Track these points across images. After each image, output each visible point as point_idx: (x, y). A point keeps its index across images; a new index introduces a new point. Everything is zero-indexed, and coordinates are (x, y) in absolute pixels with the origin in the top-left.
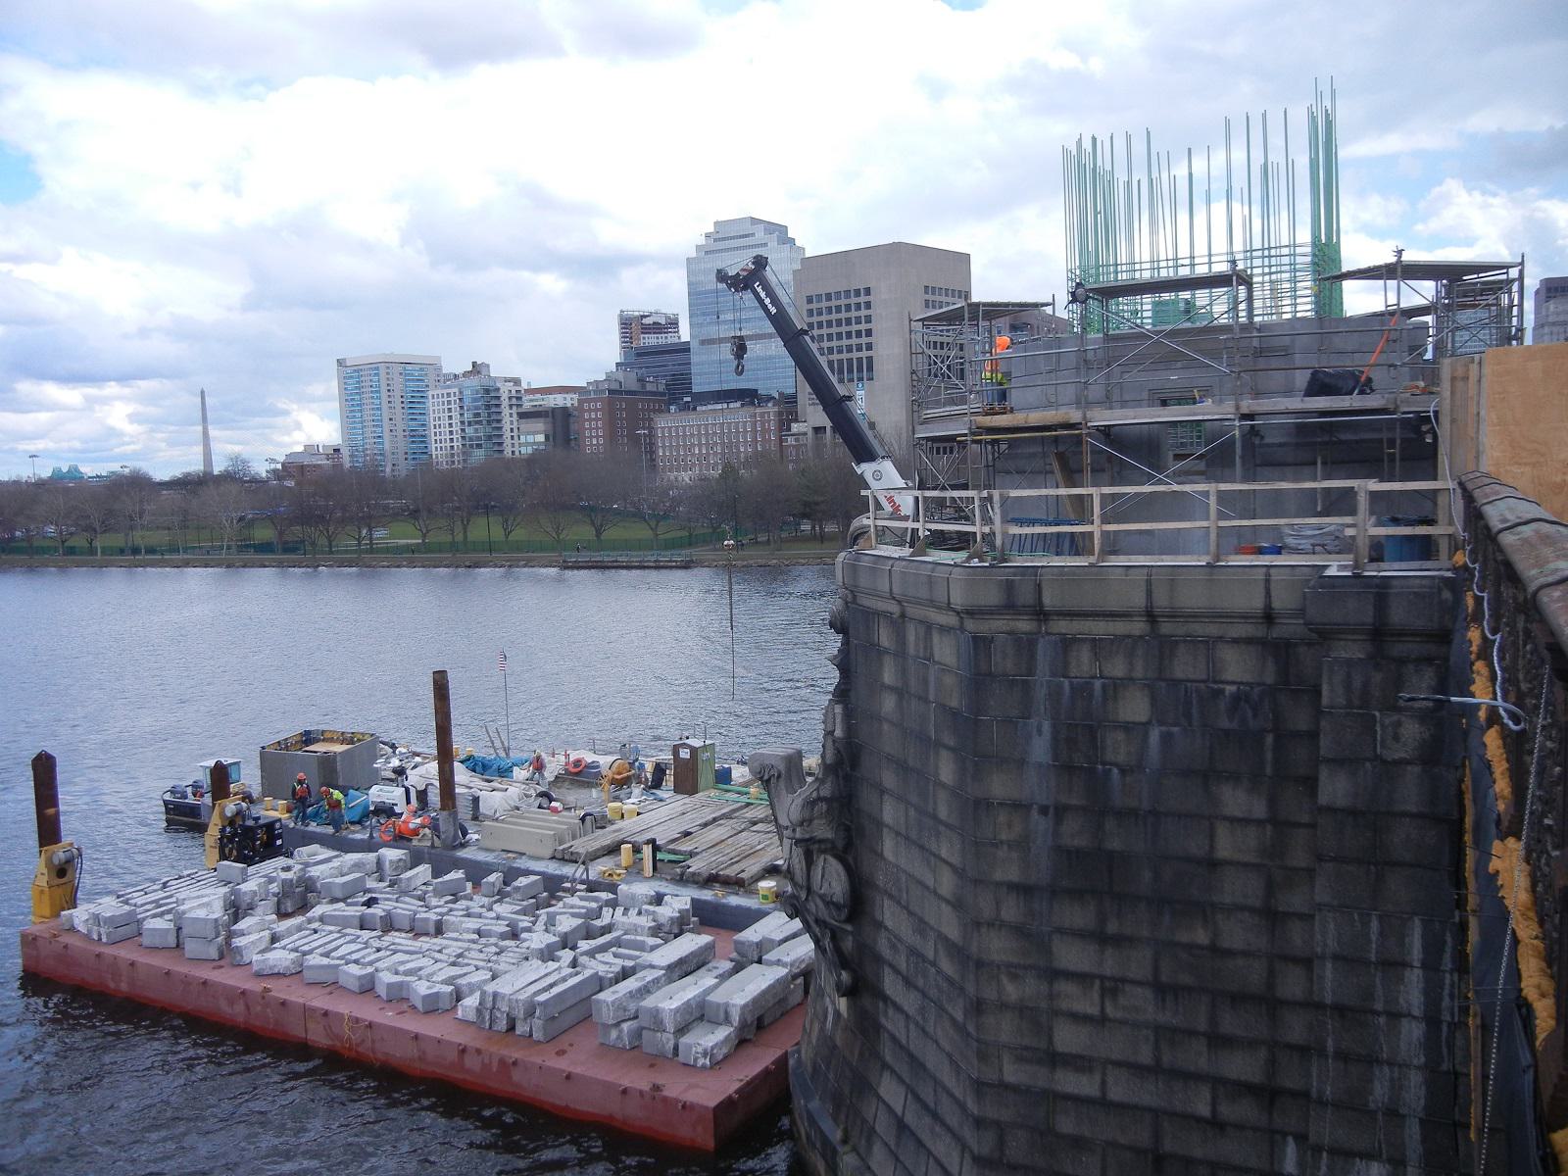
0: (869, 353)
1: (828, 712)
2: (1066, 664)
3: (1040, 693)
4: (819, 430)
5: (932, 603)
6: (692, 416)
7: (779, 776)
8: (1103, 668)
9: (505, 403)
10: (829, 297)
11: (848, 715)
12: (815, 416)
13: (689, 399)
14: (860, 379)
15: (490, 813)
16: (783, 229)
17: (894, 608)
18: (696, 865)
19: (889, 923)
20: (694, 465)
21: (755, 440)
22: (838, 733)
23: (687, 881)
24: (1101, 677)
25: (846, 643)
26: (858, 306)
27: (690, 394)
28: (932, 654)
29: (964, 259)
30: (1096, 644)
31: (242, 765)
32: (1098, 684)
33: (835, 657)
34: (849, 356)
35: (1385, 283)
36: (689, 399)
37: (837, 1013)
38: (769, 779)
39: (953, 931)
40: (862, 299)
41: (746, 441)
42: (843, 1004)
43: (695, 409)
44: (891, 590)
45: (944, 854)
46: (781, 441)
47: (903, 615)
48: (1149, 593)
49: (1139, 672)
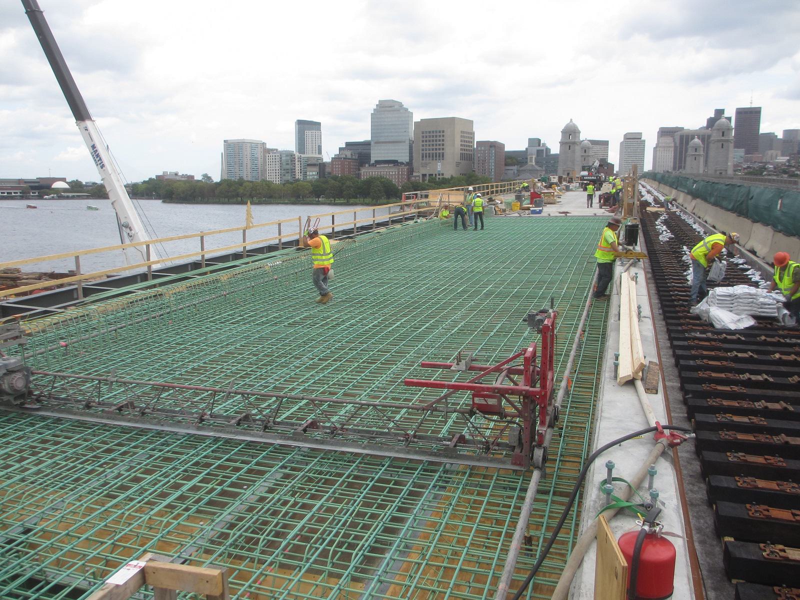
10: (430, 132)
21: (399, 178)
26: (440, 136)
29: (472, 122)
31: (503, 163)
35: (249, 215)
40: (441, 134)
41: (395, 178)
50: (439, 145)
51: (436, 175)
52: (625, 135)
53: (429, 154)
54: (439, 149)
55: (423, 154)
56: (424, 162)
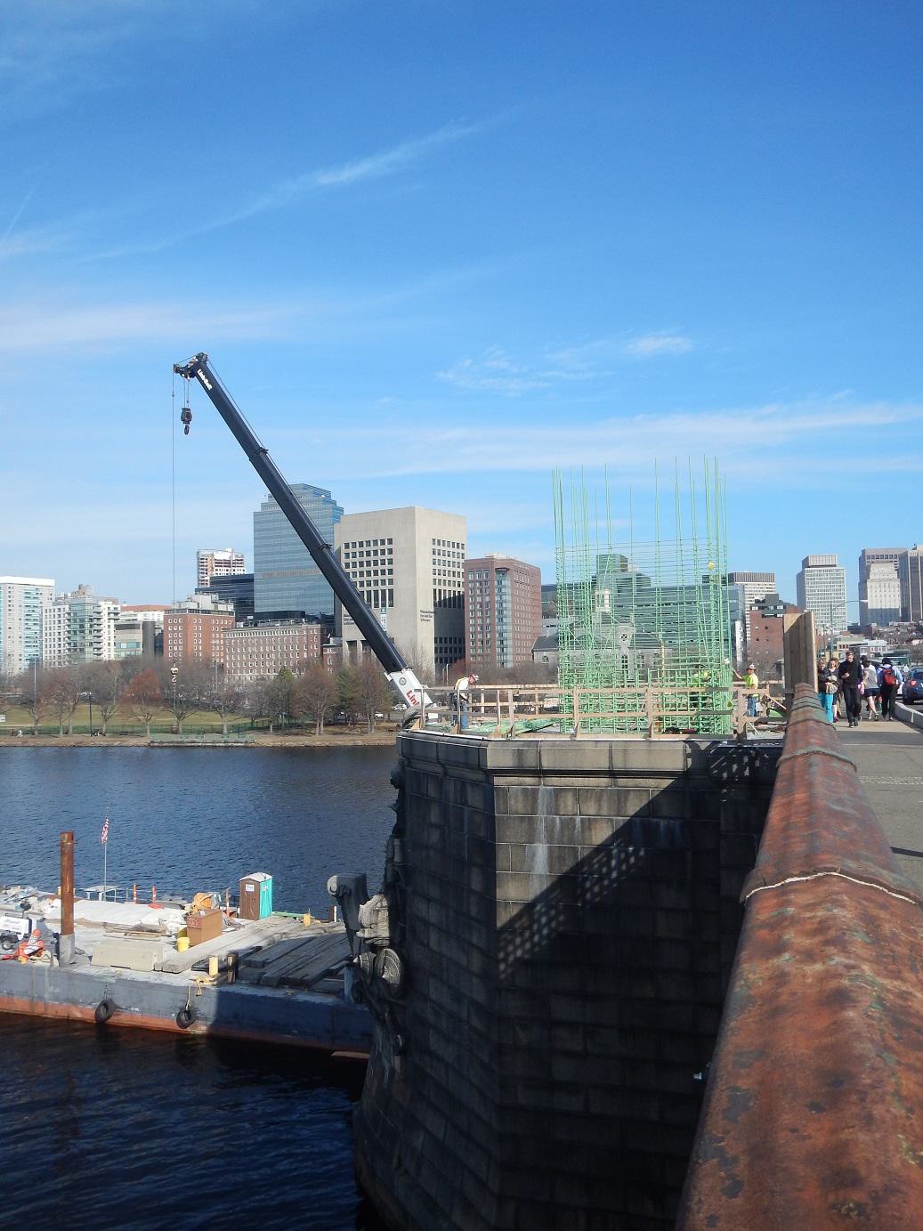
0: (391, 587)
1: (390, 848)
2: (557, 806)
3: (541, 827)
4: (352, 643)
5: (467, 766)
6: (255, 630)
7: (350, 894)
8: (582, 809)
9: (105, 617)
11: (403, 847)
12: (351, 632)
13: (252, 617)
15: (507, 761)
16: (328, 494)
17: (439, 769)
18: (270, 972)
19: (433, 996)
20: (254, 668)
22: (397, 859)
23: (263, 985)
24: (581, 815)
25: (402, 796)
27: (252, 613)
28: (466, 801)
30: (577, 793)
32: (578, 819)
33: (395, 805)
34: (376, 588)
36: (252, 617)
37: (393, 1070)
38: (343, 896)
39: (480, 996)
42: (397, 1061)
43: (256, 625)
44: (437, 757)
45: (475, 940)
46: (322, 651)
47: (446, 774)
48: (611, 758)
49: (605, 811)
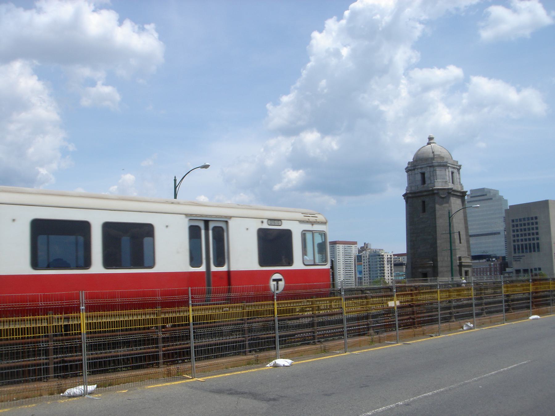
0: (538, 241)
10: (520, 220)
14: (534, 251)
50: (533, 234)
51: (531, 270)
52: (406, 169)
53: (518, 246)
54: (533, 239)
55: (514, 246)
56: (517, 255)
